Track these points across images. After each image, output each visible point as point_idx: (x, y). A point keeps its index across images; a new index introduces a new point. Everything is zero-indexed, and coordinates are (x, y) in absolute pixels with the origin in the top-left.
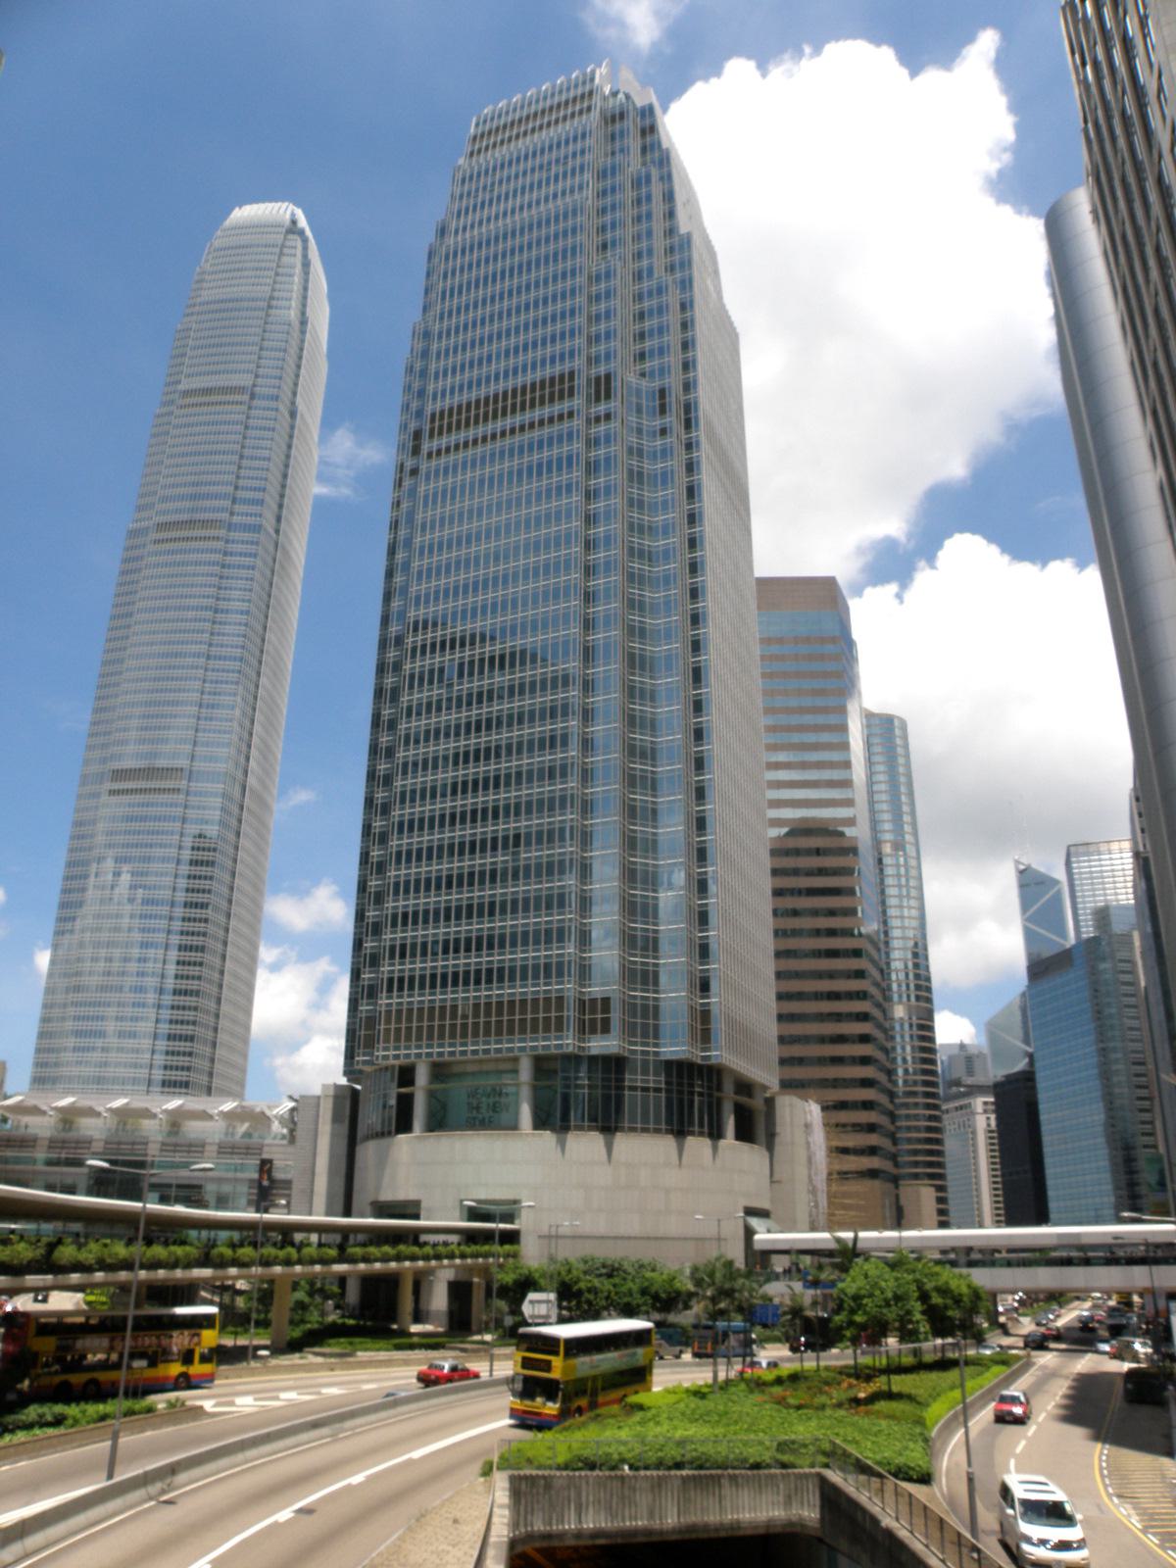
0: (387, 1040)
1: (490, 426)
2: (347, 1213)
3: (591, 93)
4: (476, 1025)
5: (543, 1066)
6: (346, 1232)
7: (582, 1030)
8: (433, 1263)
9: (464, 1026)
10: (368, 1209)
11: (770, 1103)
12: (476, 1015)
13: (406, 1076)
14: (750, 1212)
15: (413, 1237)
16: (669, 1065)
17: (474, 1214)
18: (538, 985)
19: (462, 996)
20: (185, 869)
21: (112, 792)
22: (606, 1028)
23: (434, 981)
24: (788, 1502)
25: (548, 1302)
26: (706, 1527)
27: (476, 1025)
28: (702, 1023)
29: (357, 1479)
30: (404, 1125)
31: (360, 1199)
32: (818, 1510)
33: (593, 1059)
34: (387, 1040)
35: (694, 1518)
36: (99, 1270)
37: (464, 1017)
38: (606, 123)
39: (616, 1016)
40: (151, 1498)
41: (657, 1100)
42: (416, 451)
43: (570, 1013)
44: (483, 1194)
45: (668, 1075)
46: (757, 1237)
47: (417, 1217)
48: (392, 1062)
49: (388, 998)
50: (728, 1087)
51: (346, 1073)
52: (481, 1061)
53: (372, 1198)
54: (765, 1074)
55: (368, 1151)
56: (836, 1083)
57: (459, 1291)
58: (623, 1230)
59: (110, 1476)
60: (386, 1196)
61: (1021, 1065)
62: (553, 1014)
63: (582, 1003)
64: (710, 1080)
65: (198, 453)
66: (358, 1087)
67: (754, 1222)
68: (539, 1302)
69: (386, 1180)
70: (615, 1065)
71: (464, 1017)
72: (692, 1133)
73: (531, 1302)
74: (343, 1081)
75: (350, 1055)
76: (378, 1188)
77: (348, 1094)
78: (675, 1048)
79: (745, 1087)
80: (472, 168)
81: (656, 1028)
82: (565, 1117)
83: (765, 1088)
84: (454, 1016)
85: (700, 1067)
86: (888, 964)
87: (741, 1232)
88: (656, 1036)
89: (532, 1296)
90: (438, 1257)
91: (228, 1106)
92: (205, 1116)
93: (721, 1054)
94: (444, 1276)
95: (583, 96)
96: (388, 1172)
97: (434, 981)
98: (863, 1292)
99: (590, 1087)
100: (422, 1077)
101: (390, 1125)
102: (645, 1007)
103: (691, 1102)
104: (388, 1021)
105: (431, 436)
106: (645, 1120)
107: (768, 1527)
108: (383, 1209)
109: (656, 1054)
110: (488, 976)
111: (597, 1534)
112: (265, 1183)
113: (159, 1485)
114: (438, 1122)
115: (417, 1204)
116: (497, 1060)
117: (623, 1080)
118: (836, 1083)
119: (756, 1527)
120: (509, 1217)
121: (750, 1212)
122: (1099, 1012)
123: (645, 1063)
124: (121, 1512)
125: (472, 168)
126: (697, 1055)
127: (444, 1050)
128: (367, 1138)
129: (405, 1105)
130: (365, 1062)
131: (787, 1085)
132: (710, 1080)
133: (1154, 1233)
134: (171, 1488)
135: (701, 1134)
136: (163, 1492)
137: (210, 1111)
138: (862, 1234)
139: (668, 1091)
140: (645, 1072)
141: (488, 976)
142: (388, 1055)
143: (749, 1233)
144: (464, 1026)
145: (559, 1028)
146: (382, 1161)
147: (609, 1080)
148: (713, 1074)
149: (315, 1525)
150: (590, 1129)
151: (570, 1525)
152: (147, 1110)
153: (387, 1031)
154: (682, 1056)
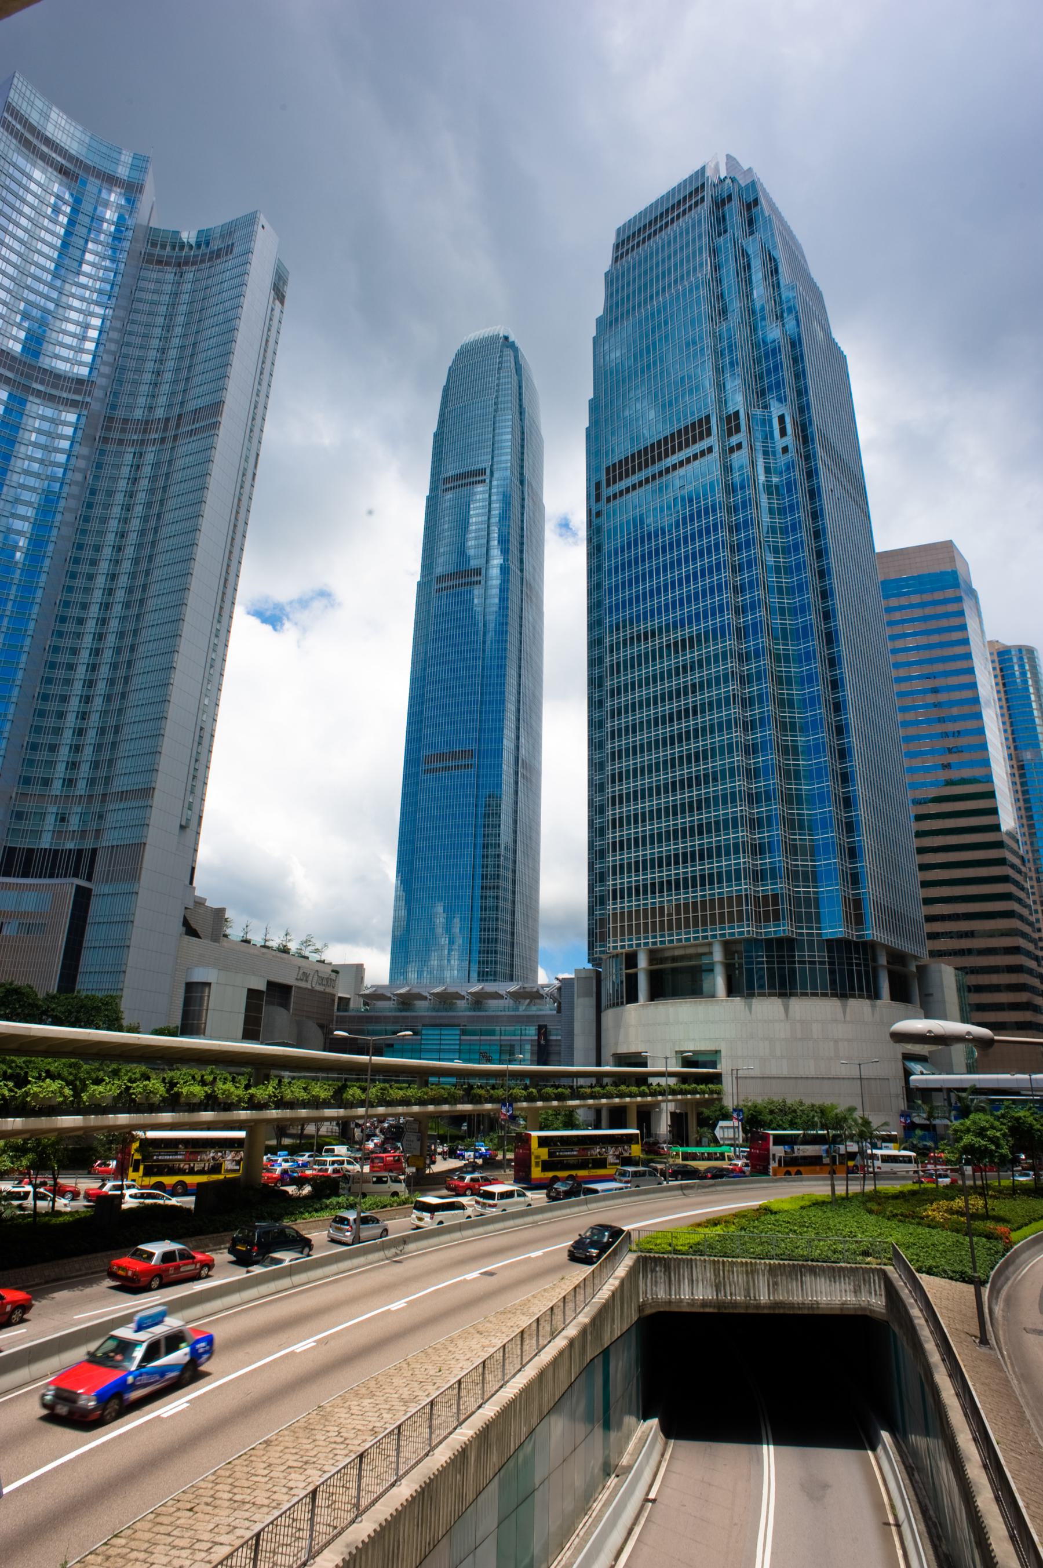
0: (615, 935)
1: (669, 460)
2: (599, 1064)
3: (703, 185)
5: (729, 947)
6: (599, 1076)
8: (660, 1098)
9: (670, 921)
10: (611, 1059)
11: (922, 970)
12: (678, 913)
13: (631, 960)
15: (642, 1080)
16: (832, 945)
17: (687, 1062)
18: (731, 886)
19: (669, 900)
20: (481, 821)
21: (426, 772)
23: (655, 888)
24: (857, 1291)
25: (734, 1127)
26: (792, 1305)
27: (678, 920)
30: (632, 998)
31: (607, 1054)
32: (883, 1299)
33: (769, 942)
34: (615, 935)
35: (781, 1297)
36: (416, 1105)
37: (670, 915)
38: (718, 208)
39: (784, 906)
40: (387, 1259)
41: (822, 970)
42: (598, 498)
44: (692, 1046)
45: (830, 951)
47: (645, 1065)
48: (619, 950)
49: (614, 904)
50: (883, 960)
51: (589, 961)
52: (685, 947)
53: (613, 1052)
54: (919, 950)
55: (609, 1016)
56: (961, 953)
57: (678, 1119)
58: (801, 1073)
60: (623, 1049)
63: (757, 899)
64: (865, 953)
68: (728, 1127)
69: (621, 1038)
70: (787, 944)
71: (670, 915)
72: (853, 996)
73: (721, 1127)
74: (590, 966)
75: (591, 946)
76: (616, 1044)
77: (593, 975)
78: (835, 929)
79: (898, 958)
80: (617, 270)
81: (818, 914)
82: (750, 987)
83: (916, 958)
84: (662, 914)
85: (856, 944)
87: (901, 1073)
88: (818, 921)
89: (721, 1123)
90: (662, 1094)
91: (513, 987)
92: (497, 996)
93: (873, 933)
94: (668, 1107)
95: (697, 190)
96: (622, 1031)
97: (655, 888)
99: (794, 962)
100: (643, 962)
101: (622, 997)
102: (807, 900)
103: (851, 972)
104: (615, 921)
105: (608, 485)
106: (814, 986)
107: (841, 1309)
108: (622, 1059)
109: (819, 935)
110: (706, 880)
111: (704, 1303)
112: (543, 1042)
113: (393, 1251)
114: (657, 993)
116: (696, 946)
117: (794, 956)
118: (961, 953)
119: (832, 1309)
120: (714, 1065)
123: (811, 943)
124: (364, 1266)
125: (617, 270)
126: (853, 934)
128: (607, 1008)
129: (632, 982)
130: (602, 952)
131: (934, 954)
132: (865, 953)
133: (979, 1080)
134: (402, 1252)
135: (861, 997)
136: (397, 1255)
137: (500, 992)
138: (1034, 1076)
139: (831, 963)
140: (811, 949)
141: (706, 880)
142: (616, 945)
144: (670, 921)
146: (618, 1025)
147: (783, 956)
148: (868, 948)
149: (492, 1282)
150: (771, 995)
151: (686, 1295)
152: (419, 994)
153: (615, 928)
154: (839, 936)
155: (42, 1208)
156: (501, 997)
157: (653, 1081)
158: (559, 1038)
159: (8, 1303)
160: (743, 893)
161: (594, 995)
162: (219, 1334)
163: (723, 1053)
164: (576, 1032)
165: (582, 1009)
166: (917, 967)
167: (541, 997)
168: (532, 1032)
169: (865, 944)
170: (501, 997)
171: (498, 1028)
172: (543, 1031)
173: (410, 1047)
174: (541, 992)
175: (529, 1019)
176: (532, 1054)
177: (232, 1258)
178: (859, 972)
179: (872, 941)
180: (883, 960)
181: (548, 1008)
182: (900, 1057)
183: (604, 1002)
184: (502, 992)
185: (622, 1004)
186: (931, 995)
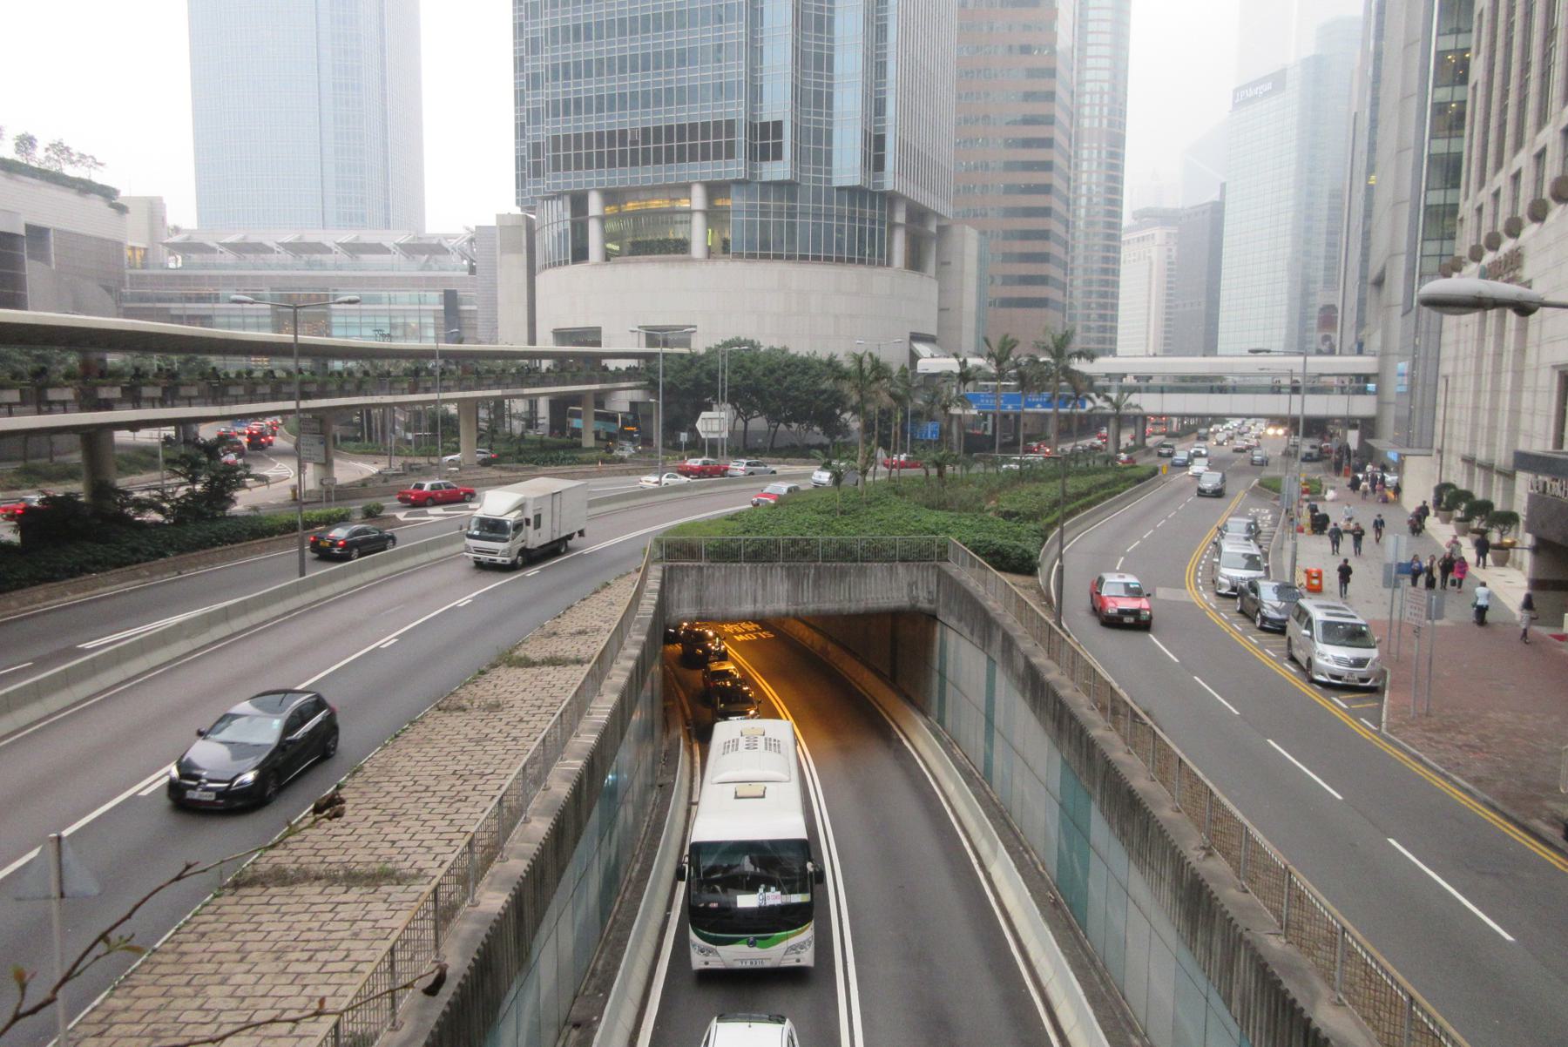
4: (646, 151)
7: (752, 157)
11: (943, 230)
14: (916, 337)
22: (778, 156)
28: (876, 149)
29: (387, 641)
43: (741, 138)
46: (920, 362)
51: (517, 204)
55: (544, 280)
59: (302, 574)
61: (1214, 196)
62: (687, 143)
65: (1526, 67)
66: (533, 217)
67: (921, 348)
71: (634, 143)
74: (517, 211)
79: (918, 215)
83: (939, 216)
84: (623, 142)
86: (1081, 83)
89: (704, 414)
93: (890, 182)
98: (230, 891)
100: (595, 205)
101: (566, 255)
115: (597, 331)
121: (916, 337)
122: (976, 215)
127: (618, 177)
128: (540, 272)
137: (386, 244)
143: (914, 357)
145: (730, 155)
148: (890, 199)
155: (113, 363)
156: (386, 251)
157: (612, 364)
158: (474, 308)
159: (1371, 393)
160: (605, 170)
161: (525, 251)
162: (1398, 592)
163: (699, 330)
164: (500, 300)
165: (512, 269)
166: (938, 227)
167: (446, 251)
168: (434, 301)
169: (883, 195)
170: (386, 251)
171: (385, 294)
172: (451, 299)
173: (254, 320)
174: (445, 244)
175: (430, 283)
176: (436, 328)
177: (316, 555)
178: (872, 232)
179: (893, 191)
180: (900, 217)
181: (455, 268)
182: (907, 336)
183: (539, 261)
184: (388, 244)
185: (566, 263)
186: (949, 263)
